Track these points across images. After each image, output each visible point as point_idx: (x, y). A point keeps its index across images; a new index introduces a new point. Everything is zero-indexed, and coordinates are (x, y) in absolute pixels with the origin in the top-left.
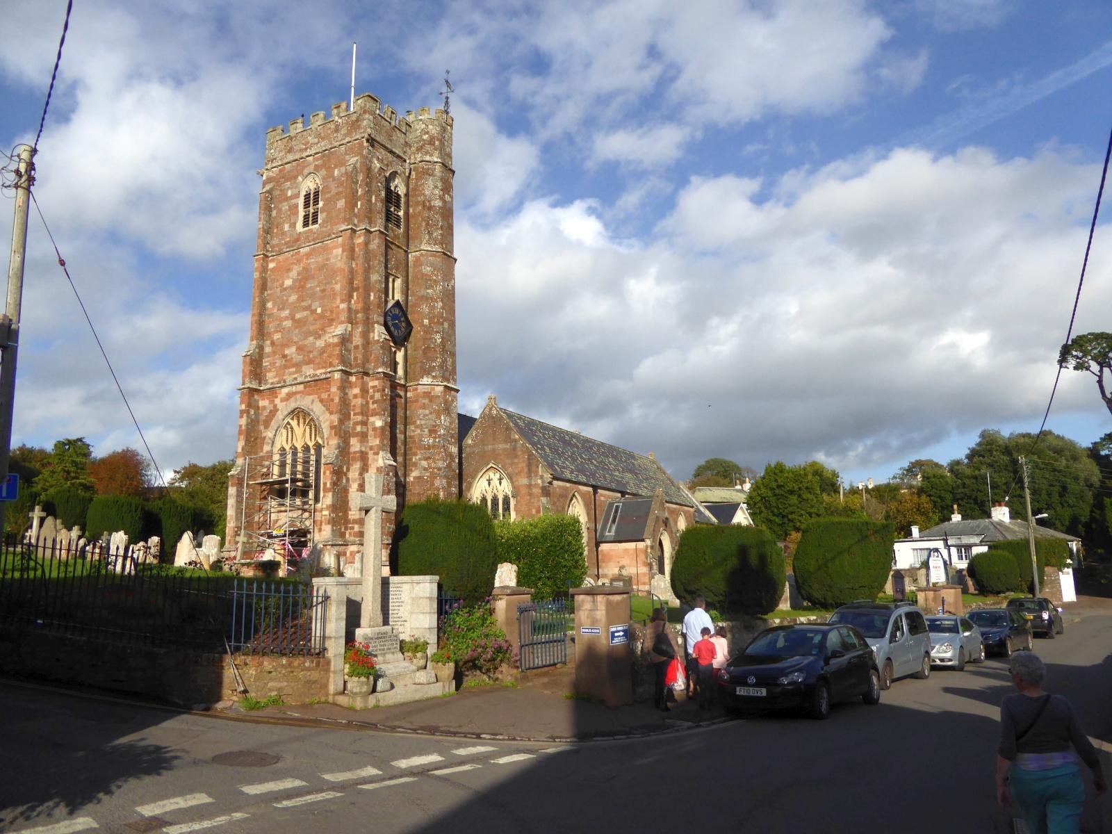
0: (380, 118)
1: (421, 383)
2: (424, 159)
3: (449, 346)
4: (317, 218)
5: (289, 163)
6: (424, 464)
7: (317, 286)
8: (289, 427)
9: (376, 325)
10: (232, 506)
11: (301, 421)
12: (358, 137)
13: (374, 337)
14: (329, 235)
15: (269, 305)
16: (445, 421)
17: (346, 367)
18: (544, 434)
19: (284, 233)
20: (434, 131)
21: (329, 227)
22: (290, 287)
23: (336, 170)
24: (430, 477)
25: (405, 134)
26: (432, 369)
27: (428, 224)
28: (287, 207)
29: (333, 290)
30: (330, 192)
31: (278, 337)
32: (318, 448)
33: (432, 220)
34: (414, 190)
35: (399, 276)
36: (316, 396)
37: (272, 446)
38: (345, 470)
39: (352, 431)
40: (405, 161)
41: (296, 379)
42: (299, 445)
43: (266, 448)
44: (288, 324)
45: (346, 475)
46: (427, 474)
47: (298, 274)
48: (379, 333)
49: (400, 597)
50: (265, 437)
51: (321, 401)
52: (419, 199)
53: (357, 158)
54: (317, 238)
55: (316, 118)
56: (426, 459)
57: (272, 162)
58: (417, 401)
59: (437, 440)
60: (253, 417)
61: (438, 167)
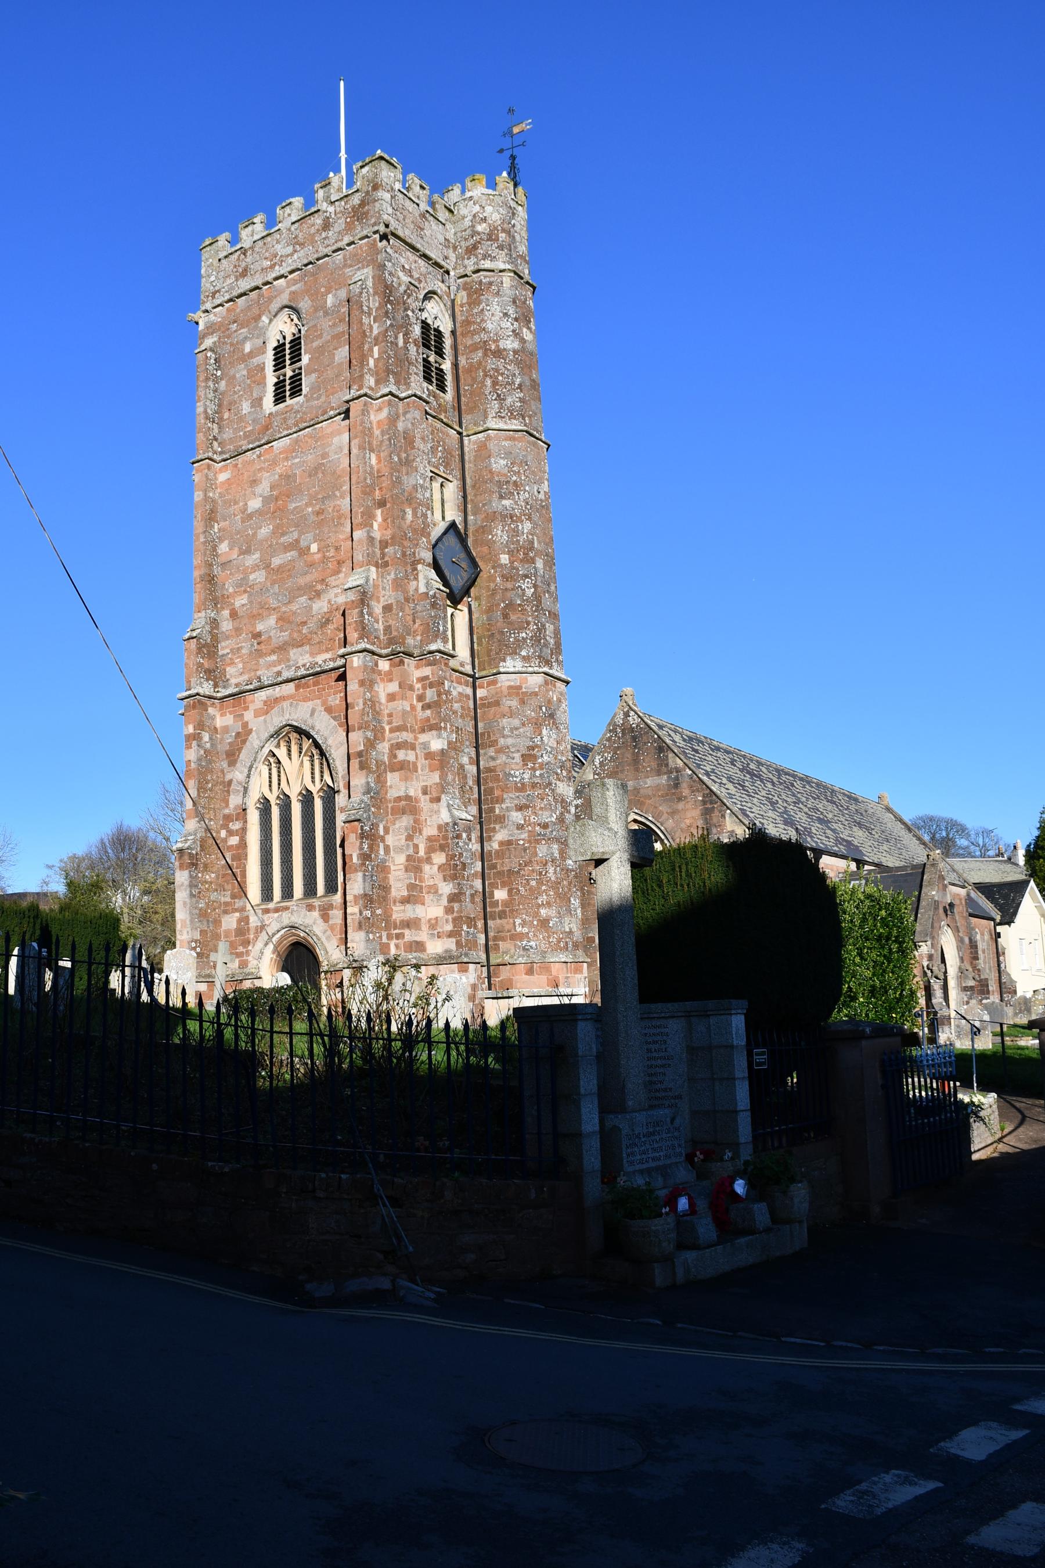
0: (401, 196)
1: (502, 670)
2: (482, 267)
3: (547, 601)
4: (301, 385)
5: (244, 294)
6: (517, 817)
7: (307, 505)
8: (272, 760)
9: (420, 567)
10: (185, 903)
11: (294, 748)
12: (365, 233)
13: (417, 590)
14: (325, 412)
15: (223, 547)
16: (550, 737)
17: (373, 644)
18: (717, 759)
19: (241, 419)
20: (496, 217)
21: (323, 398)
22: (259, 512)
23: (330, 296)
24: (529, 842)
25: (444, 225)
26: (520, 644)
27: (495, 383)
28: (245, 372)
29: (337, 509)
30: (320, 336)
31: (243, 602)
32: (330, 794)
33: (502, 374)
34: (467, 323)
35: (450, 477)
36: (319, 701)
37: (244, 797)
38: (382, 833)
39: (390, 760)
40: (448, 272)
41: (279, 673)
42: (294, 793)
43: (235, 800)
44: (258, 577)
45: (383, 840)
46: (523, 836)
47: (272, 488)
48: (427, 580)
49: (663, 1047)
50: (230, 782)
51: (329, 710)
52: (477, 338)
53: (366, 271)
54: (302, 420)
55: (288, 210)
56: (520, 808)
57: (213, 297)
58: (497, 703)
59: (538, 773)
60: (208, 745)
61: (507, 280)
